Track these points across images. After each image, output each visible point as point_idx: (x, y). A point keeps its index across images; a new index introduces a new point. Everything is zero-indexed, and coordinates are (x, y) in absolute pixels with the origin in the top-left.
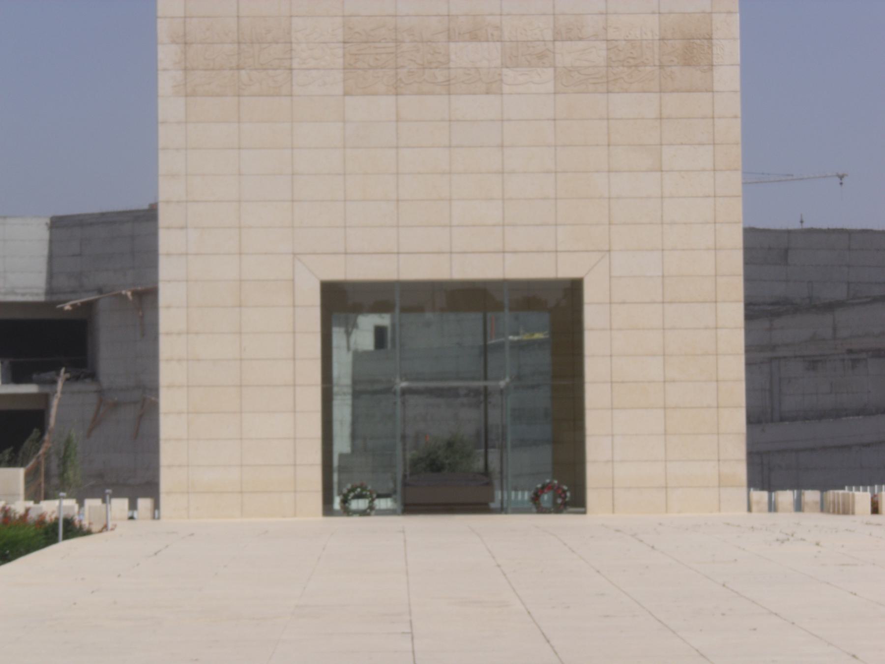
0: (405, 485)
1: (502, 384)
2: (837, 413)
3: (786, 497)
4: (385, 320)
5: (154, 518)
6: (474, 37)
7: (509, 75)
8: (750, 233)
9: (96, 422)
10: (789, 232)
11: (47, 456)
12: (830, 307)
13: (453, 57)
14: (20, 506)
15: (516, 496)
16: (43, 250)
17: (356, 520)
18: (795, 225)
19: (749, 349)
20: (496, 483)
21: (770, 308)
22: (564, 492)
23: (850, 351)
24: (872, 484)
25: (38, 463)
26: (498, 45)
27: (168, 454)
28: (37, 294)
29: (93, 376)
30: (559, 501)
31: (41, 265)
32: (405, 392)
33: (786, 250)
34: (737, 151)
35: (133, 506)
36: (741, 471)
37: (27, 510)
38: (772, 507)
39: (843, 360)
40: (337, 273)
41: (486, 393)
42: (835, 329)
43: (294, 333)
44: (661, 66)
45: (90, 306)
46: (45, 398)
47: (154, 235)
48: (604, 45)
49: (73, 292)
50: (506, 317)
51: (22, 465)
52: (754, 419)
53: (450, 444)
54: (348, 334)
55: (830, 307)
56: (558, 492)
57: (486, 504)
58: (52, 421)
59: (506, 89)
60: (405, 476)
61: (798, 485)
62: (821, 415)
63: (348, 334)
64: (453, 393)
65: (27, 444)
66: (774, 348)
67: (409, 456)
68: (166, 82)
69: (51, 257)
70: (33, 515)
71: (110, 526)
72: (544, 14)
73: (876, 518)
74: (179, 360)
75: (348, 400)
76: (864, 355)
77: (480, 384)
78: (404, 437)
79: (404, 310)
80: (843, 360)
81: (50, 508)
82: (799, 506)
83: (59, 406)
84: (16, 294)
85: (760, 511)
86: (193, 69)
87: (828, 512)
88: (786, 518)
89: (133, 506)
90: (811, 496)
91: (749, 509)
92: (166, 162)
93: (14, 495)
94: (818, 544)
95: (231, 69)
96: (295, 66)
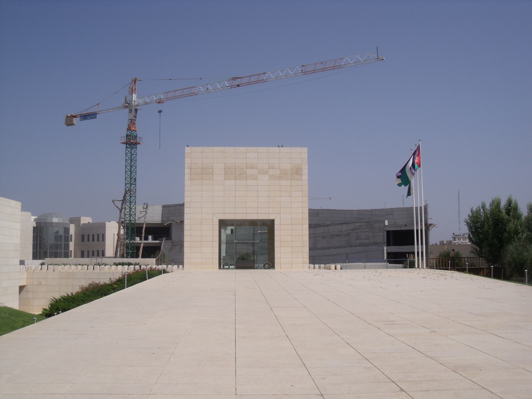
0: (236, 263)
1: (257, 241)
2: (329, 248)
3: (317, 266)
4: (233, 228)
5: (183, 269)
6: (252, 168)
7: (514, 225)
8: (310, 210)
9: (172, 249)
10: (319, 210)
11: (161, 256)
12: (327, 226)
13: (247, 172)
14: (154, 266)
15: (261, 265)
16: (160, 212)
17: (226, 270)
18: (320, 208)
19: (309, 234)
20: (256, 263)
21: (315, 226)
22: (270, 265)
23: (331, 235)
24: (336, 263)
25: (159, 257)
26: (257, 170)
27: (186, 256)
28: (160, 222)
29: (171, 239)
30: (269, 267)
31: (161, 215)
32: (236, 243)
33: (318, 213)
34: (307, 193)
35: (178, 267)
36: (308, 260)
37: (156, 267)
38: (314, 268)
39: (330, 237)
40: (222, 218)
41: (254, 243)
42: (328, 230)
43: (213, 230)
44: (291, 175)
45: (170, 224)
46: (161, 244)
47: (184, 209)
48: (279, 170)
49: (167, 221)
50: (258, 227)
51: (155, 258)
52: (311, 249)
53: (246, 254)
54: (225, 231)
55: (327, 226)
56: (269, 265)
57: (254, 267)
58: (162, 248)
59: (258, 179)
60: (236, 261)
61: (320, 263)
62: (325, 248)
63: (225, 231)
64: (248, 243)
65: (156, 253)
66: (315, 234)
67: (237, 257)
68: (187, 177)
69: (162, 214)
70: (157, 268)
71: (173, 271)
72: (266, 164)
73: (336, 270)
74: (188, 236)
75: (225, 245)
76: (334, 236)
77: (253, 241)
78: (236, 253)
79: (236, 226)
80: (330, 237)
81: (160, 267)
82: (320, 268)
83: (163, 245)
84: (155, 221)
85: (312, 269)
86: (192, 174)
87: (326, 269)
88: (317, 270)
89: (178, 267)
90: (322, 266)
91: (309, 269)
92: (186, 194)
93: (153, 264)
94: (323, 276)
95: (200, 174)
96: (214, 174)
